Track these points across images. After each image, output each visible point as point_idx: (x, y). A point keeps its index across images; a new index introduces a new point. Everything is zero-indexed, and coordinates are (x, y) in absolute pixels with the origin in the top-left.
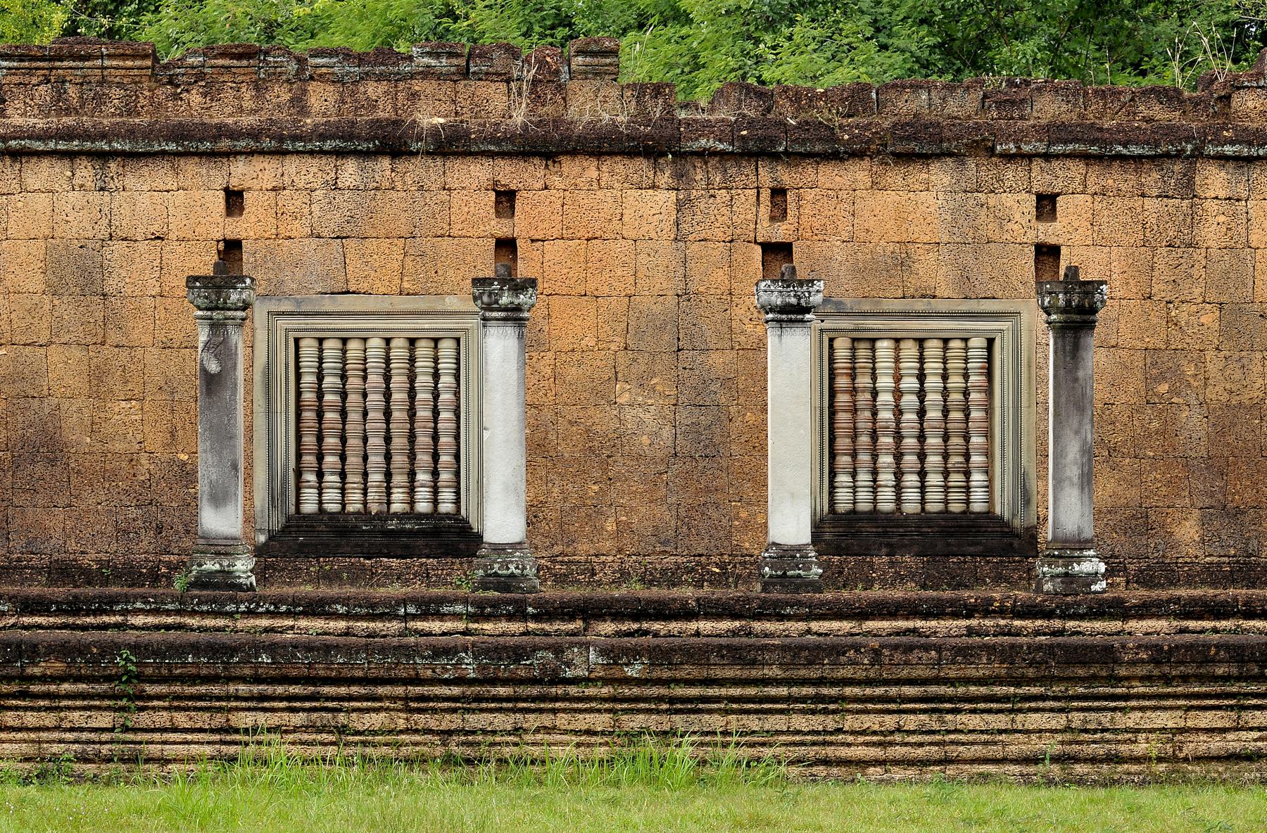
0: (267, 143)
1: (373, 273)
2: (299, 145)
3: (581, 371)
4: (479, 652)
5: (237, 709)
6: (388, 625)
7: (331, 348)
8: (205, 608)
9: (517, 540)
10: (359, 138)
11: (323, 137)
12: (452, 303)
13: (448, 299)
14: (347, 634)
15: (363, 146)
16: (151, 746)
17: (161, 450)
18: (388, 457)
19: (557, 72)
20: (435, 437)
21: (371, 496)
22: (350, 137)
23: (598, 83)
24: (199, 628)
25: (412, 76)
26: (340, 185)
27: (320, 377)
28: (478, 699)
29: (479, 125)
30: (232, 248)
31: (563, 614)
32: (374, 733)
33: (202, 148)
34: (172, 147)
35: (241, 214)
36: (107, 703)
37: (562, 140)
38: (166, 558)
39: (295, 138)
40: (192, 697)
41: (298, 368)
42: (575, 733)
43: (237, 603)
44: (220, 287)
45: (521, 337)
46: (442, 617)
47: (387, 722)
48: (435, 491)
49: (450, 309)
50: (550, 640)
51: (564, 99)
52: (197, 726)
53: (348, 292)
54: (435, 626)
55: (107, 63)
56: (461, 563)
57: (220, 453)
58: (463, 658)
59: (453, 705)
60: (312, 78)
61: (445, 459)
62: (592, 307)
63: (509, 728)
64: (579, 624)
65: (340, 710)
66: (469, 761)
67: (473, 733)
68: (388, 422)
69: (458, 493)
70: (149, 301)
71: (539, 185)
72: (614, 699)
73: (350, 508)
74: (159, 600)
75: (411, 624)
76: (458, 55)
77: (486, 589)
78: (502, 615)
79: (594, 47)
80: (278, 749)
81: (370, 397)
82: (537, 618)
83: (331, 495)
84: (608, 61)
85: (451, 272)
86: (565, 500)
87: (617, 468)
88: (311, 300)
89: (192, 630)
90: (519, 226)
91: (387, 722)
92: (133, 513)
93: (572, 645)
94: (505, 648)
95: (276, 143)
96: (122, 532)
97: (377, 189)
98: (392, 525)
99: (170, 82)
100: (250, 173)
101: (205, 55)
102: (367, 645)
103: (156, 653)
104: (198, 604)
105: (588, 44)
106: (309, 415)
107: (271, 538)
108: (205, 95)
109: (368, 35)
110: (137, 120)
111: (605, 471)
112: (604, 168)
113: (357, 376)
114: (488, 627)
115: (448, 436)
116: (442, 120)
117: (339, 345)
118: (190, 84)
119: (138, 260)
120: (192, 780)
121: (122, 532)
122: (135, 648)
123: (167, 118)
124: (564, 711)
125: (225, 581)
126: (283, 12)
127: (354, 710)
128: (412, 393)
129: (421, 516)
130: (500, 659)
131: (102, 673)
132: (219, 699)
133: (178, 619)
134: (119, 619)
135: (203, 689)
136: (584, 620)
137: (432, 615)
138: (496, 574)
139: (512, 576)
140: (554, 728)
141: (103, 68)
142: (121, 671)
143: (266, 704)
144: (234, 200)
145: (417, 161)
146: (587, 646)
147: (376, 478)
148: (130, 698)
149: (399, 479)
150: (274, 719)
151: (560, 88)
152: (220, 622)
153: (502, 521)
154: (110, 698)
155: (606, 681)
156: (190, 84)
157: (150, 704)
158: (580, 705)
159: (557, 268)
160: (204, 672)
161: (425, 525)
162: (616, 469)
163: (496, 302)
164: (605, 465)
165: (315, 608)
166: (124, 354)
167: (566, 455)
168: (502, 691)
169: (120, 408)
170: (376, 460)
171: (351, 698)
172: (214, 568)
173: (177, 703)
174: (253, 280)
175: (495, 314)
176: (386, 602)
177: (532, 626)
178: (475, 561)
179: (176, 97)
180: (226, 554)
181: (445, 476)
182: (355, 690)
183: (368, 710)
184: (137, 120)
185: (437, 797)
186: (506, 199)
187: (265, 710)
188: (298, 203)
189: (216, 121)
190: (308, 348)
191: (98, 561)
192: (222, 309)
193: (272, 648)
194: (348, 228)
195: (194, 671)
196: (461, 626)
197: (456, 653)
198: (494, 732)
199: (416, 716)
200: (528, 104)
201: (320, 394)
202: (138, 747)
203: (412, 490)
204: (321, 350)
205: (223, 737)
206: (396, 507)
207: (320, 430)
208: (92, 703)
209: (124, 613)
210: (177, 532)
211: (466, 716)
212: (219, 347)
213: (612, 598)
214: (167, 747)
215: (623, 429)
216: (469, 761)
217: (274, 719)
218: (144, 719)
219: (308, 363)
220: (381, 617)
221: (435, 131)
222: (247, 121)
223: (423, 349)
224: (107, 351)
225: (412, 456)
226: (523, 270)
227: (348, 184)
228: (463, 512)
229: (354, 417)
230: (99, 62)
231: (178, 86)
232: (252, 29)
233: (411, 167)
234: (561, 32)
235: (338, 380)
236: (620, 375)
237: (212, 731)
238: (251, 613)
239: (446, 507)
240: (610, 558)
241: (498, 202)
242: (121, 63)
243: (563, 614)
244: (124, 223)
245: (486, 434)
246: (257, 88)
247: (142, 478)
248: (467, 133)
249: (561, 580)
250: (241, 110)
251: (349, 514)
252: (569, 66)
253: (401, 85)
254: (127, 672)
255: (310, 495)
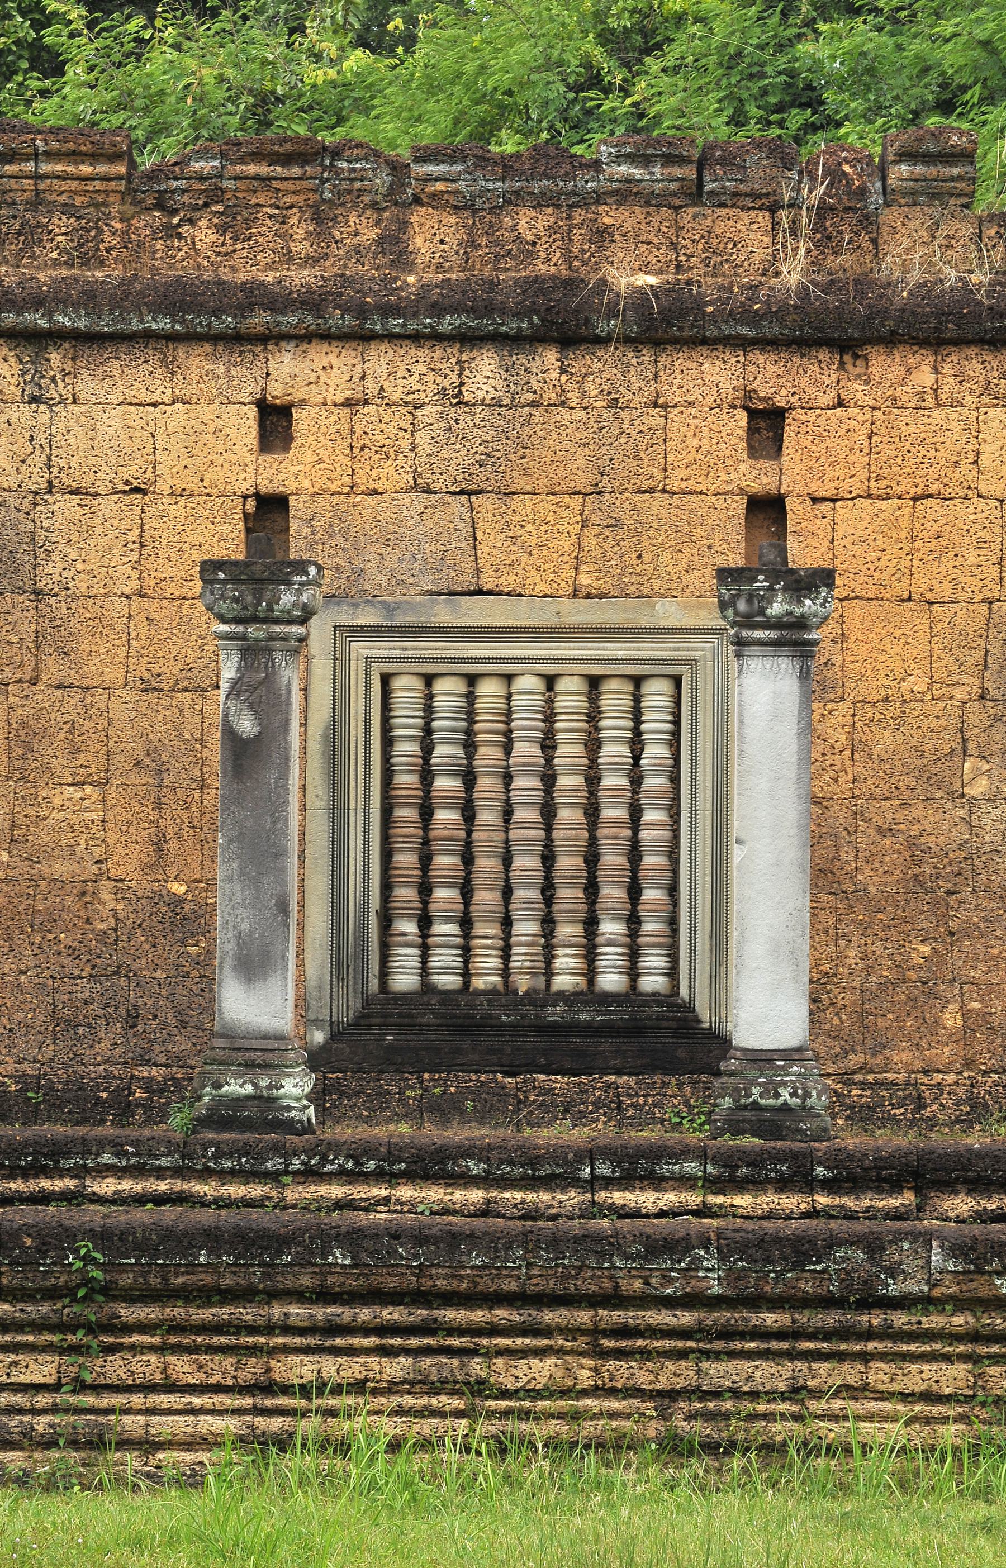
0: (336, 319)
1: (525, 558)
2: (395, 323)
3: (899, 738)
4: (729, 1247)
5: (287, 1350)
6: (559, 1196)
7: (448, 691)
8: (227, 1164)
9: (794, 1043)
10: (503, 311)
11: (438, 310)
12: (667, 612)
13: (660, 605)
14: (485, 1211)
15: (511, 326)
16: (126, 1419)
17: (137, 875)
18: (548, 890)
19: (862, 192)
20: (635, 854)
21: (517, 961)
22: (488, 310)
23: (936, 211)
24: (216, 1201)
25: (599, 198)
26: (468, 397)
27: (427, 742)
28: (727, 1334)
29: (721, 288)
30: (269, 509)
31: (880, 1179)
32: (536, 1394)
33: (218, 327)
34: (164, 324)
35: (287, 449)
36: (47, 1337)
37: (870, 318)
38: (144, 1072)
39: (388, 311)
40: (204, 1328)
41: (386, 727)
42: (906, 1397)
43: (287, 1157)
44: (261, 581)
45: (804, 675)
46: (658, 1183)
47: (559, 1374)
48: (634, 954)
49: (664, 623)
50: (859, 1227)
51: (874, 241)
52: (212, 1380)
53: (480, 592)
54: (647, 1199)
55: (45, 168)
56: (680, 1085)
57: (256, 883)
58: (701, 1259)
59: (680, 1344)
60: (417, 200)
61: (652, 895)
62: (922, 620)
63: (782, 1386)
64: (908, 1198)
65: (474, 1352)
66: (710, 1447)
67: (716, 1395)
68: (548, 827)
69: (673, 958)
70: (119, 605)
71: (828, 399)
72: (975, 1337)
73: (479, 983)
74: (144, 1150)
75: (602, 1196)
76: (682, 161)
77: (737, 1132)
78: (768, 1180)
79: (930, 146)
80: (368, 1424)
81: (519, 782)
82: (830, 1186)
83: (445, 957)
84: (955, 171)
85: (666, 557)
86: (869, 970)
87: (969, 911)
88: (412, 607)
89: (204, 1204)
90: (792, 473)
91: (559, 1374)
92: (84, 989)
93: (899, 1237)
94: (777, 1240)
95: (352, 319)
96: (64, 1024)
97: (534, 404)
98: (555, 1014)
99: (160, 206)
100: (310, 375)
101: (223, 155)
102: (525, 1234)
103: (142, 1247)
104: (215, 1157)
105: (920, 140)
106: (406, 815)
107: (334, 1036)
108: (222, 229)
109: (445, 122)
110: (99, 274)
111: (943, 920)
112: (947, 369)
113: (495, 744)
114: (743, 1201)
115: (657, 853)
116: (652, 280)
117: (461, 687)
118: (196, 208)
119: (99, 530)
120: (193, 1480)
121: (64, 1024)
122: (103, 1237)
123: (155, 270)
124: (883, 1356)
125: (264, 1114)
126: (284, 77)
127: (500, 1352)
128: (593, 778)
129: (607, 998)
130: (768, 1261)
131: (40, 1283)
132: (253, 1330)
133: (179, 1185)
134: (70, 1183)
135: (224, 1313)
136: (917, 1190)
137: (641, 1178)
138: (755, 1106)
139: (785, 1108)
140: (865, 1387)
141: (37, 177)
142: (76, 1279)
143: (339, 1341)
144: (275, 422)
145: (608, 353)
146: (926, 1238)
147: (526, 928)
148: (91, 1329)
149: (568, 931)
150: (353, 1369)
151: (868, 221)
152: (256, 1191)
153: (765, 1008)
154: (52, 1329)
155: (961, 1304)
156: (196, 208)
157: (127, 1340)
158: (912, 1347)
159: (858, 550)
160: (228, 1281)
161: (614, 1014)
162: (963, 915)
163: (762, 612)
164: (942, 910)
165: (429, 1166)
166: (72, 701)
167: (872, 889)
168: (771, 1319)
169: (64, 801)
170: (527, 895)
171: (493, 1330)
172: (242, 1091)
173: (176, 1339)
174: (320, 568)
175: (759, 634)
176: (558, 1154)
177: (823, 1200)
178: (717, 1083)
179: (171, 232)
180: (266, 1066)
181: (651, 927)
182: (502, 1314)
183: (524, 1353)
184: (99, 274)
185: (643, 1509)
186: (767, 426)
187: (336, 1351)
188: (391, 429)
189: (242, 277)
190: (407, 690)
191: (20, 1078)
192: (265, 621)
193: (354, 1239)
194: (481, 475)
195: (209, 1279)
196: (693, 1199)
197: (688, 1248)
198: (754, 1395)
199: (612, 1364)
200: (808, 251)
201: (427, 776)
202: (101, 1419)
203: (590, 954)
204: (430, 697)
205: (258, 1401)
206: (563, 982)
207: (426, 842)
208: (19, 1338)
209: (80, 1172)
210: (164, 1025)
211: (704, 1365)
212: (258, 689)
213: (970, 1150)
214: (156, 1419)
215: (975, 843)
216: (710, 1447)
217: (353, 1369)
218: (116, 1368)
219: (407, 719)
220: (548, 1182)
221: (640, 297)
222: (300, 277)
223: (614, 697)
224: (41, 695)
225: (592, 889)
226: (802, 554)
227: (481, 394)
228: (684, 991)
229: (487, 817)
230: (29, 167)
231: (174, 212)
232: (231, 108)
233: (596, 365)
234: (797, 118)
235: (458, 751)
236: (971, 745)
237: (242, 1390)
238: (311, 1174)
239: (652, 982)
240: (951, 1078)
241: (752, 430)
242: (71, 169)
243: (880, 1179)
244: (75, 459)
245: (737, 854)
246: (318, 218)
247: (102, 926)
248: (699, 303)
249: (863, 1116)
250: (288, 258)
251: (478, 993)
252: (884, 179)
253: (579, 215)
254: (87, 1282)
255: (406, 960)
